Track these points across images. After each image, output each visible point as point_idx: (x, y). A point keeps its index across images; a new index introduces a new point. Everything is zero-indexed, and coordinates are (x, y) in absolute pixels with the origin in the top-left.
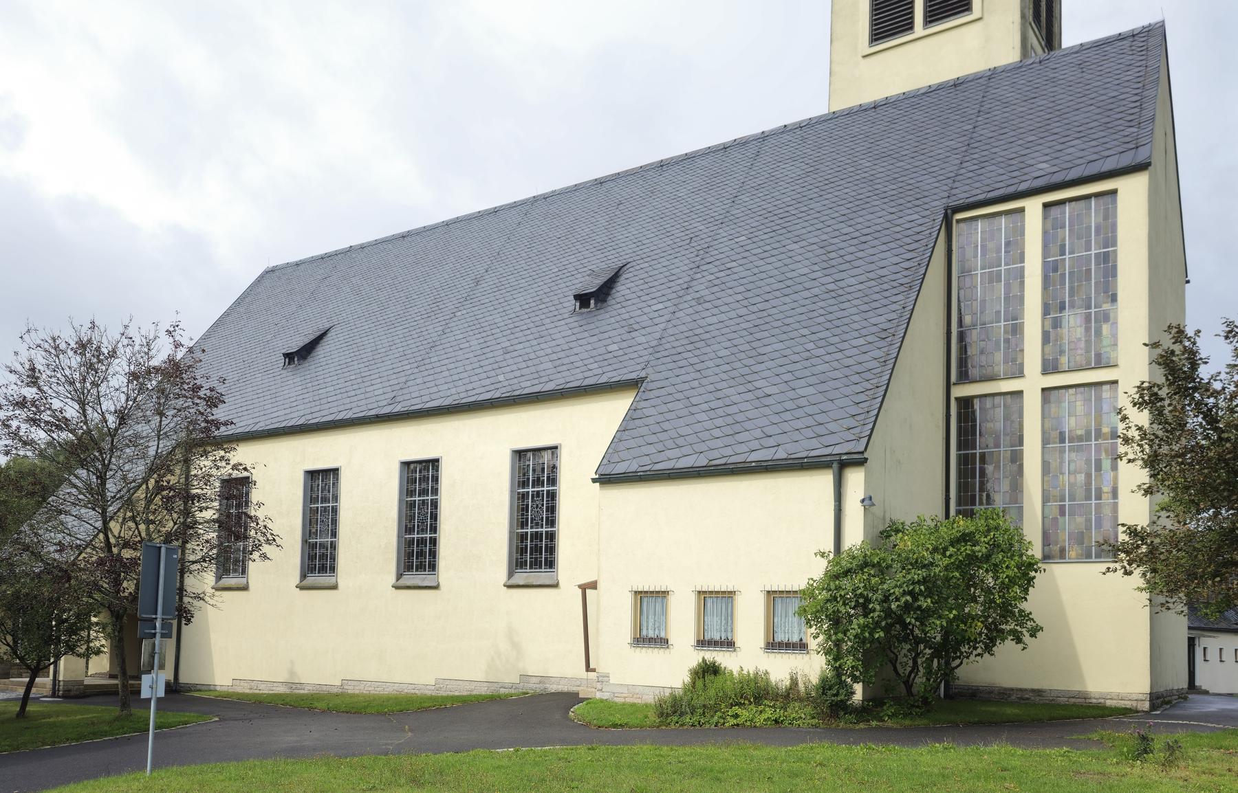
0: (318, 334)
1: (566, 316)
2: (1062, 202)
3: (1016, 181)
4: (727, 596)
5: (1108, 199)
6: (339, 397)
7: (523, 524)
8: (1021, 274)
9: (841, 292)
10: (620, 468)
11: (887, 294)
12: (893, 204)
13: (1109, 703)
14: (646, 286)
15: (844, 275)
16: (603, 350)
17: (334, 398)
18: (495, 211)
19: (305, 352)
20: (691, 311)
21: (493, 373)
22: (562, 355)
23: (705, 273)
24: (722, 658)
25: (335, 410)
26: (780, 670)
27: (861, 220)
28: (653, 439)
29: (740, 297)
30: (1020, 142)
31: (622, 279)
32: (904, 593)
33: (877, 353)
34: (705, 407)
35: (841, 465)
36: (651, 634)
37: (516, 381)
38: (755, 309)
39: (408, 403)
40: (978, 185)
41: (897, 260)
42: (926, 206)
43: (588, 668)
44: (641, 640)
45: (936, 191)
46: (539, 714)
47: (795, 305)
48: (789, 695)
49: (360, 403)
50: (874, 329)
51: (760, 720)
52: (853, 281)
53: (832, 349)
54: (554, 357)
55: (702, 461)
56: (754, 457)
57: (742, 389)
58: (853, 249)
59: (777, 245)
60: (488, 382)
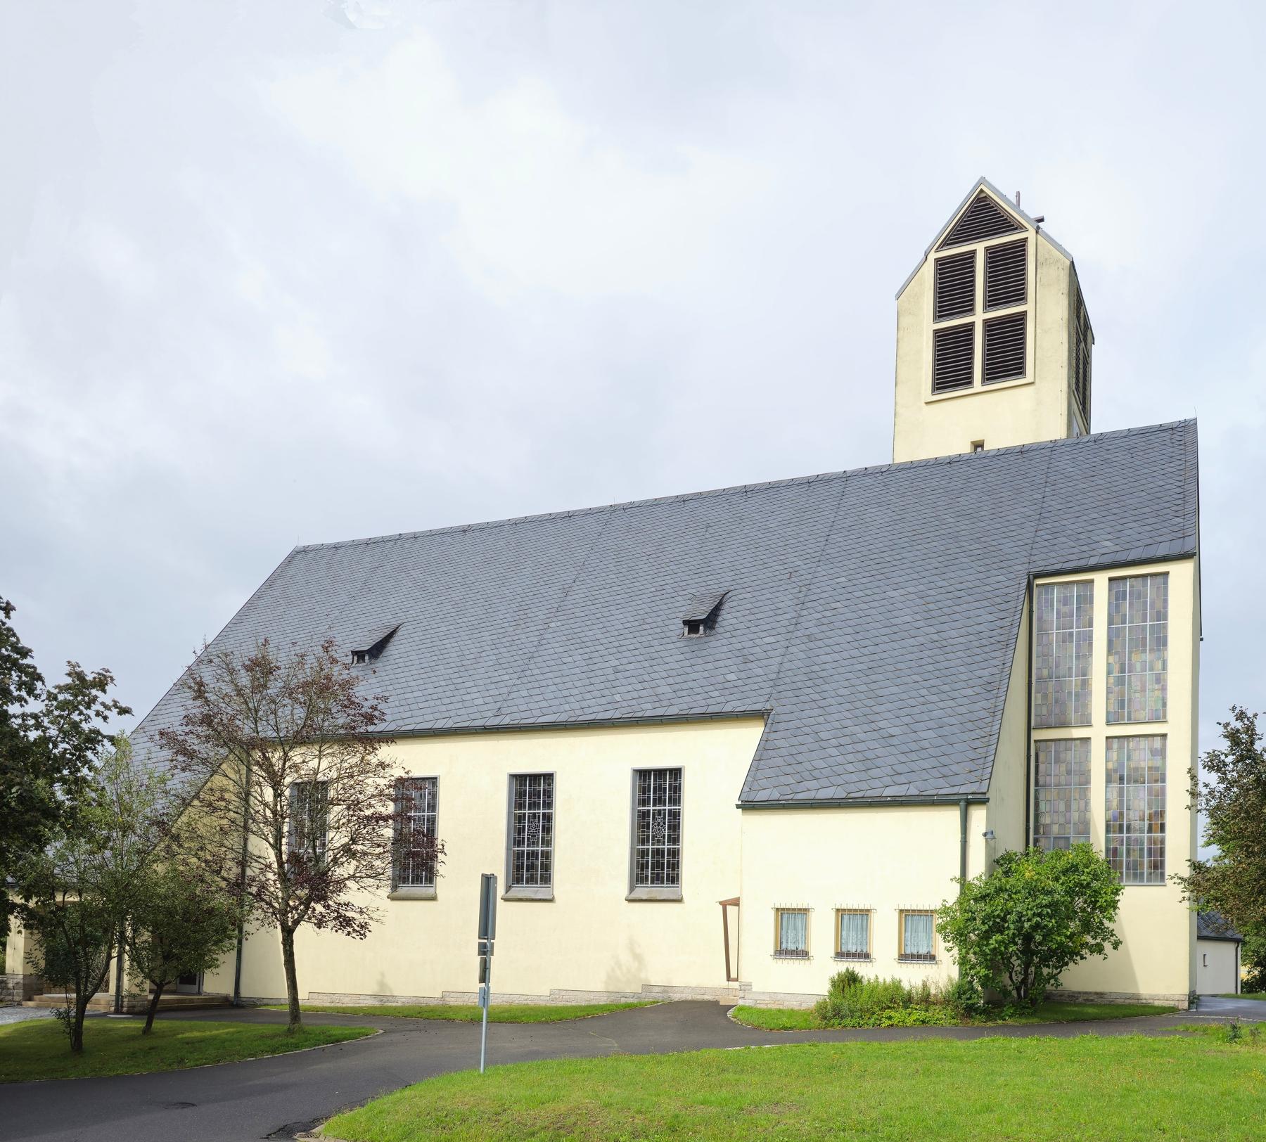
0: (387, 632)
1: (674, 639)
2: (1124, 578)
3: (1086, 555)
4: (864, 914)
5: (1160, 579)
6: (432, 703)
7: (644, 841)
8: (1089, 638)
9: (944, 643)
10: (762, 796)
11: (986, 649)
12: (980, 563)
13: (1157, 1003)
14: (752, 617)
15: (945, 627)
16: (721, 679)
17: (426, 705)
18: (570, 516)
19: (377, 650)
20: (803, 647)
21: (607, 692)
22: (678, 679)
23: (811, 611)
24: (860, 968)
25: (430, 717)
26: (913, 977)
27: (952, 575)
28: (789, 770)
29: (849, 638)
30: (1085, 518)
31: (726, 606)
32: (1034, 915)
33: (983, 704)
34: (834, 742)
35: (967, 803)
36: (792, 947)
37: (634, 702)
38: (865, 651)
39: (517, 716)
40: (1053, 554)
41: (990, 618)
42: (1011, 569)
43: (729, 978)
44: (782, 952)
45: (1017, 555)
46: (700, 1022)
47: (904, 651)
48: (926, 1000)
49: (460, 712)
50: (980, 681)
51: (909, 1021)
52: (954, 633)
53: (944, 696)
54: (671, 681)
55: (840, 793)
56: (888, 792)
57: (866, 727)
58: (949, 603)
59: (877, 591)
60: (603, 701)
